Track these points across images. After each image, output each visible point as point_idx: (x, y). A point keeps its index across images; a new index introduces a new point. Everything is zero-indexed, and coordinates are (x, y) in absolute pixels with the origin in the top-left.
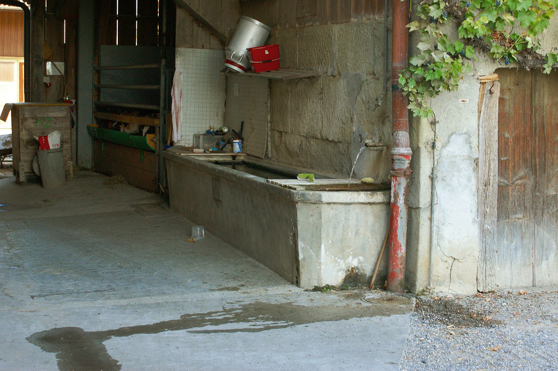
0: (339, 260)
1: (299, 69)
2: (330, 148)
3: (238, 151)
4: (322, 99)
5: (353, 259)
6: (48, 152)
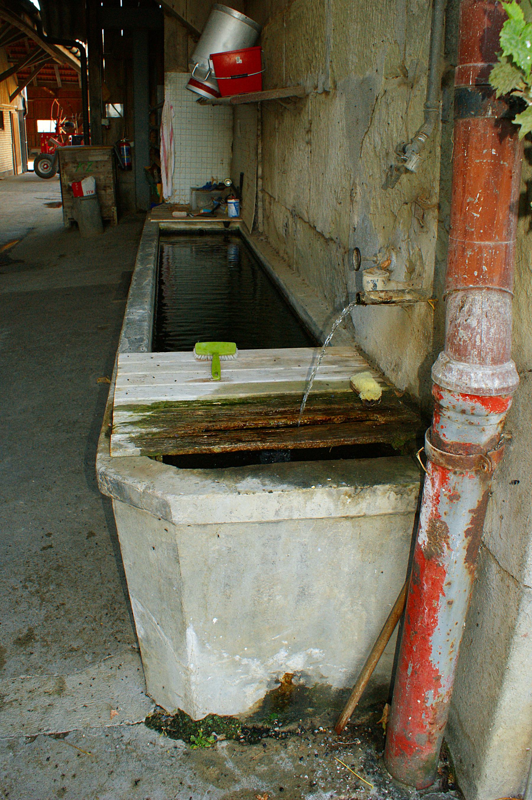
0: (245, 661)
1: (286, 87)
2: (318, 245)
3: (234, 215)
4: (309, 143)
5: (289, 655)
6: (81, 200)
